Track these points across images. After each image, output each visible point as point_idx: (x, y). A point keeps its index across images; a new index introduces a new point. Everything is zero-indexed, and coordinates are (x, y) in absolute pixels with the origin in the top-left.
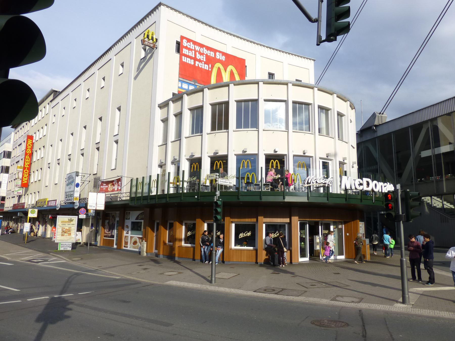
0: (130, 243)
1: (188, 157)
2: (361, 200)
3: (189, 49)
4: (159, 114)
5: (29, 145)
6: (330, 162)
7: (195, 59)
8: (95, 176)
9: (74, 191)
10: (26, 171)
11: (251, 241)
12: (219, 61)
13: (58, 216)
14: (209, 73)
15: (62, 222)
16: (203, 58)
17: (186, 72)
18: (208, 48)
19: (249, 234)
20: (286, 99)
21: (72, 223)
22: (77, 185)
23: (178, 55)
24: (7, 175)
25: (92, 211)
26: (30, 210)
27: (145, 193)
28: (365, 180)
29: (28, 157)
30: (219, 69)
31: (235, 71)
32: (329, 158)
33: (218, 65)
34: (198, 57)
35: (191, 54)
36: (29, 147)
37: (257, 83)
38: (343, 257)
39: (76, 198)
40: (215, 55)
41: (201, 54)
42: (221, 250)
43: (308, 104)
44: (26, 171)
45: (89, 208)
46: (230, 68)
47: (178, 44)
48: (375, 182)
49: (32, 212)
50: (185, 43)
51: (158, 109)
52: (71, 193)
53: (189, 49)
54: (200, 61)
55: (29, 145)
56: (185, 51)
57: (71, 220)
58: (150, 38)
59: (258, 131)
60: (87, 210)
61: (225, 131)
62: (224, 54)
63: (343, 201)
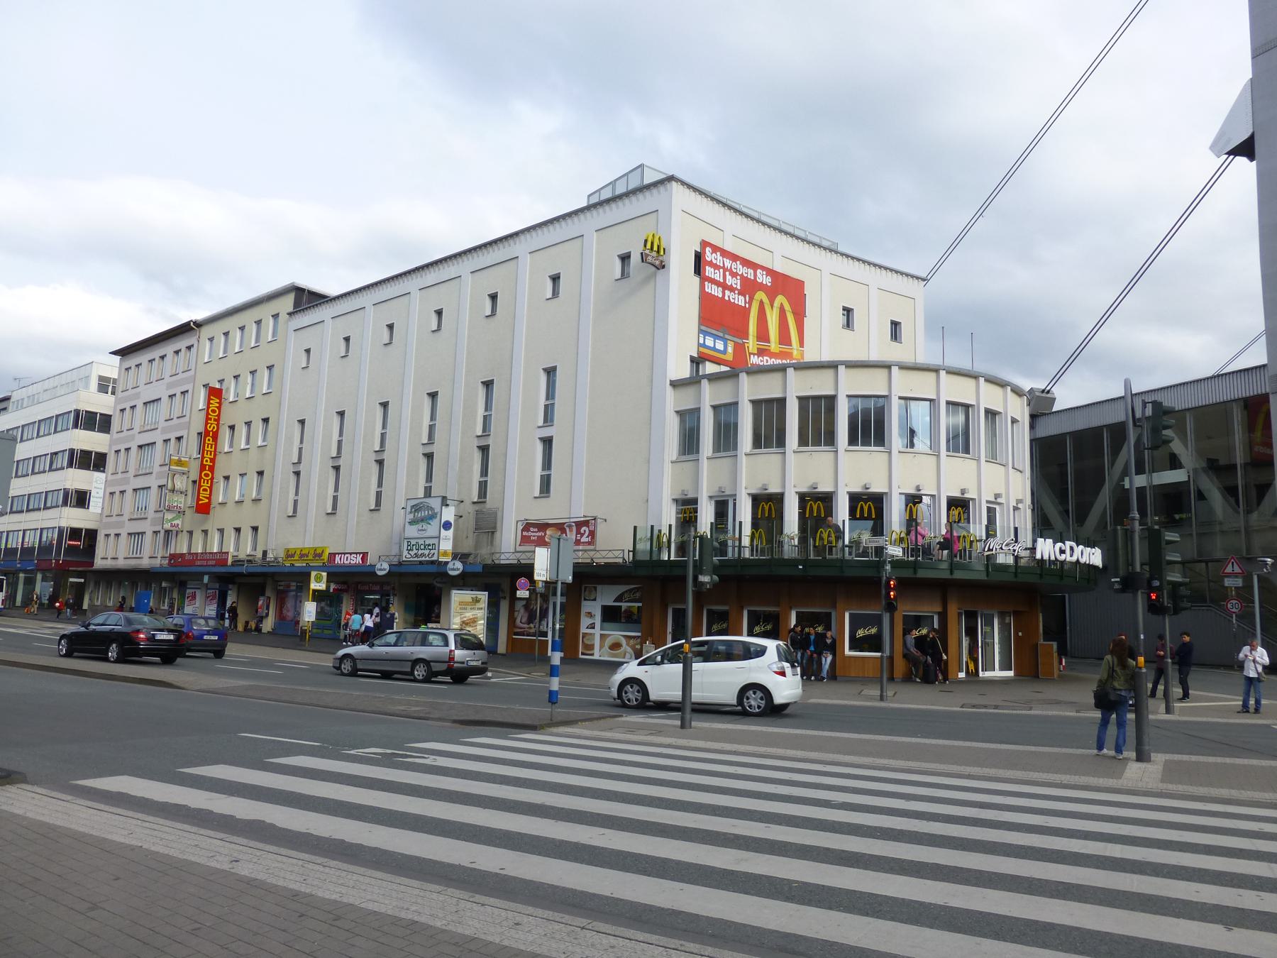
0: (601, 647)
1: (754, 491)
2: (1041, 575)
3: (716, 267)
4: (671, 402)
5: (214, 411)
6: (997, 507)
7: (724, 286)
8: (477, 507)
9: (439, 537)
10: (207, 475)
11: (873, 643)
12: (761, 287)
13: (454, 592)
14: (745, 312)
15: (461, 603)
16: (735, 282)
17: (716, 316)
18: (747, 263)
19: (874, 631)
20: (934, 397)
21: (478, 605)
22: (447, 525)
23: (697, 279)
24: (102, 475)
25: (540, 585)
26: (313, 574)
27: (643, 552)
28: (1068, 543)
29: (209, 440)
30: (761, 303)
31: (787, 307)
32: (999, 500)
33: (760, 295)
34: (730, 281)
35: (718, 276)
36: (213, 416)
37: (887, 366)
38: (1011, 674)
39: (445, 554)
40: (755, 275)
41: (734, 275)
42: (830, 658)
43: (967, 407)
44: (207, 475)
45: (536, 578)
46: (780, 299)
47: (699, 258)
48: (1081, 547)
49: (318, 580)
50: (709, 255)
51: (669, 389)
52: (435, 541)
53: (716, 267)
54: (732, 289)
55: (214, 411)
56: (709, 271)
57: (477, 601)
58: (655, 248)
59: (890, 453)
60: (533, 582)
61: (827, 448)
62: (770, 272)
63: (1008, 578)
